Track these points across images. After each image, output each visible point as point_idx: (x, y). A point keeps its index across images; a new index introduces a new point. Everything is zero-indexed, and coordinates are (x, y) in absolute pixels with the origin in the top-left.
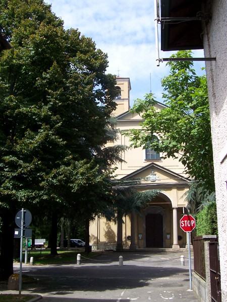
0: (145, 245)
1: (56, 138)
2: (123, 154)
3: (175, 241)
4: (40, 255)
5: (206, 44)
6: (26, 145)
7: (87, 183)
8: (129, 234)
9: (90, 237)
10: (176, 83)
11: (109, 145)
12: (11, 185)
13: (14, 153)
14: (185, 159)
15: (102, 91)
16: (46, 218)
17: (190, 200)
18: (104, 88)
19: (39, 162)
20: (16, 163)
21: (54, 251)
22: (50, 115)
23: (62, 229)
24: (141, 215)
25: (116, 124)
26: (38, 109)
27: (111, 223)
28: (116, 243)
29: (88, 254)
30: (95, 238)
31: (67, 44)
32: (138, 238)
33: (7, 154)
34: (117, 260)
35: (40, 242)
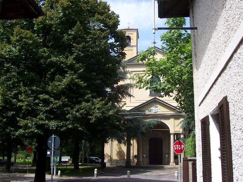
0: (148, 162)
1: (79, 81)
2: (132, 90)
3: (172, 159)
4: (66, 169)
5: (191, 14)
6: (56, 86)
7: (102, 116)
8: (136, 153)
9: (105, 156)
10: (172, 39)
11: (121, 83)
12: (44, 117)
13: (47, 93)
14: (178, 98)
15: (115, 43)
16: (70, 140)
17: (184, 127)
18: (116, 41)
19: (66, 100)
20: (49, 100)
21: (76, 166)
22: (75, 63)
23: (83, 149)
24: (145, 139)
25: (126, 67)
26: (65, 59)
27: (122, 145)
28: (125, 161)
29: (103, 169)
30: (109, 156)
31: (88, 7)
32: (143, 157)
33: (42, 93)
34: (126, 174)
35: (65, 159)
